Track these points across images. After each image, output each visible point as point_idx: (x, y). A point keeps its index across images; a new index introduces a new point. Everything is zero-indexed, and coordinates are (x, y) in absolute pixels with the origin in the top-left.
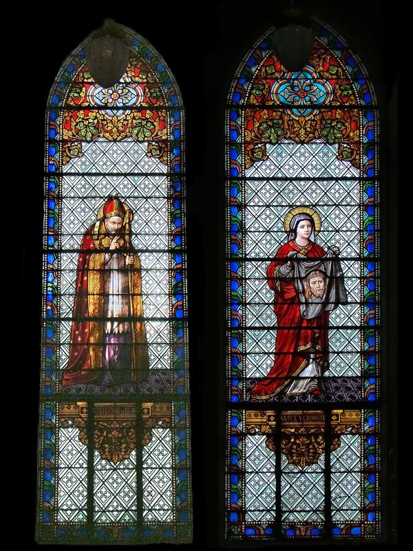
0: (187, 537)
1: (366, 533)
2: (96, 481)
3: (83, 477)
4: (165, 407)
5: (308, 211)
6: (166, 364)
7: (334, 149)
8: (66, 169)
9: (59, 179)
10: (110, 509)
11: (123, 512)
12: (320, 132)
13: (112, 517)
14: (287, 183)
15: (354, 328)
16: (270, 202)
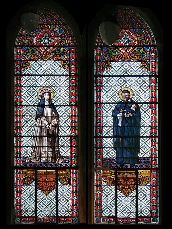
0: (157, 222)
1: (156, 218)
2: (118, 201)
3: (112, 200)
4: (148, 172)
5: (127, 89)
6: (68, 154)
7: (60, 63)
8: (104, 74)
9: (101, 78)
10: (44, 211)
11: (50, 213)
12: (57, 57)
13: (46, 214)
14: (49, 77)
15: (67, 136)
16: (131, 85)
